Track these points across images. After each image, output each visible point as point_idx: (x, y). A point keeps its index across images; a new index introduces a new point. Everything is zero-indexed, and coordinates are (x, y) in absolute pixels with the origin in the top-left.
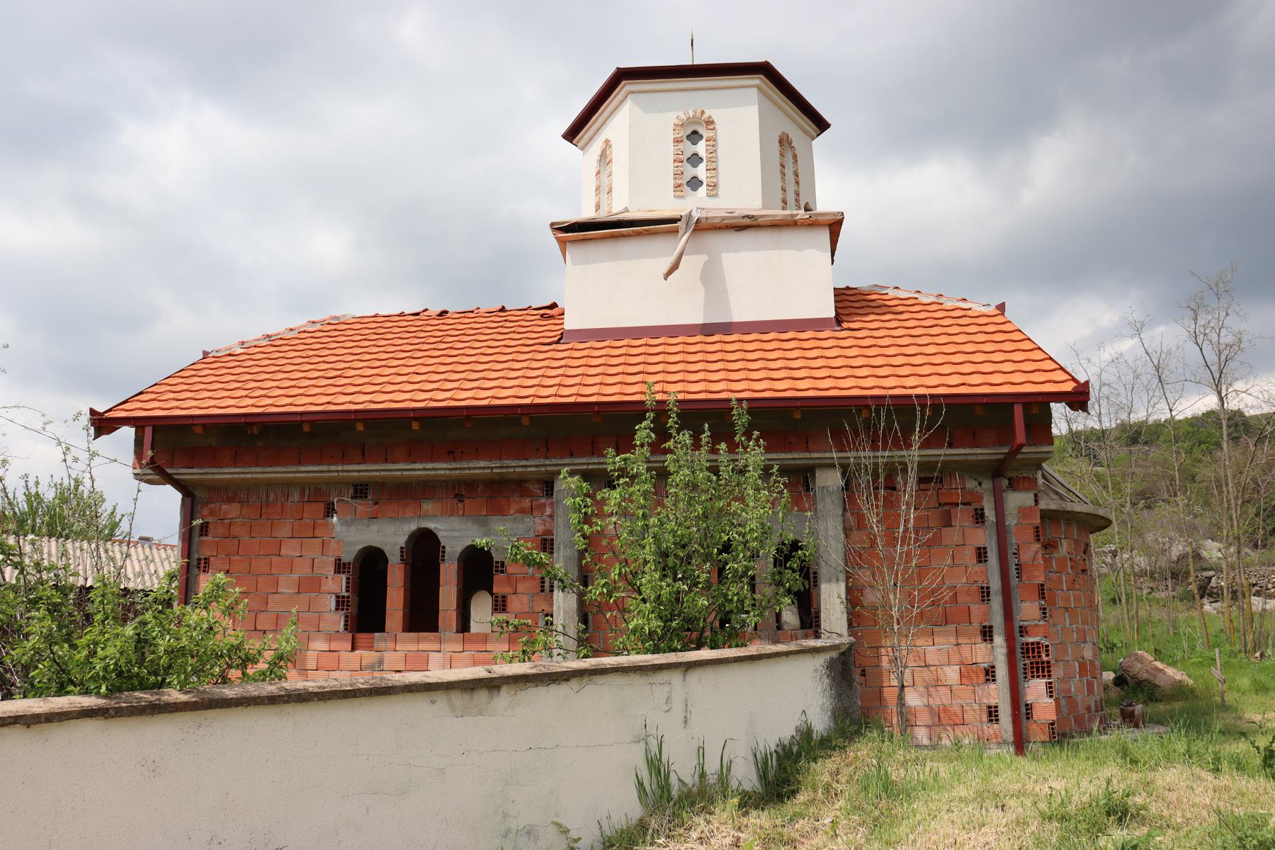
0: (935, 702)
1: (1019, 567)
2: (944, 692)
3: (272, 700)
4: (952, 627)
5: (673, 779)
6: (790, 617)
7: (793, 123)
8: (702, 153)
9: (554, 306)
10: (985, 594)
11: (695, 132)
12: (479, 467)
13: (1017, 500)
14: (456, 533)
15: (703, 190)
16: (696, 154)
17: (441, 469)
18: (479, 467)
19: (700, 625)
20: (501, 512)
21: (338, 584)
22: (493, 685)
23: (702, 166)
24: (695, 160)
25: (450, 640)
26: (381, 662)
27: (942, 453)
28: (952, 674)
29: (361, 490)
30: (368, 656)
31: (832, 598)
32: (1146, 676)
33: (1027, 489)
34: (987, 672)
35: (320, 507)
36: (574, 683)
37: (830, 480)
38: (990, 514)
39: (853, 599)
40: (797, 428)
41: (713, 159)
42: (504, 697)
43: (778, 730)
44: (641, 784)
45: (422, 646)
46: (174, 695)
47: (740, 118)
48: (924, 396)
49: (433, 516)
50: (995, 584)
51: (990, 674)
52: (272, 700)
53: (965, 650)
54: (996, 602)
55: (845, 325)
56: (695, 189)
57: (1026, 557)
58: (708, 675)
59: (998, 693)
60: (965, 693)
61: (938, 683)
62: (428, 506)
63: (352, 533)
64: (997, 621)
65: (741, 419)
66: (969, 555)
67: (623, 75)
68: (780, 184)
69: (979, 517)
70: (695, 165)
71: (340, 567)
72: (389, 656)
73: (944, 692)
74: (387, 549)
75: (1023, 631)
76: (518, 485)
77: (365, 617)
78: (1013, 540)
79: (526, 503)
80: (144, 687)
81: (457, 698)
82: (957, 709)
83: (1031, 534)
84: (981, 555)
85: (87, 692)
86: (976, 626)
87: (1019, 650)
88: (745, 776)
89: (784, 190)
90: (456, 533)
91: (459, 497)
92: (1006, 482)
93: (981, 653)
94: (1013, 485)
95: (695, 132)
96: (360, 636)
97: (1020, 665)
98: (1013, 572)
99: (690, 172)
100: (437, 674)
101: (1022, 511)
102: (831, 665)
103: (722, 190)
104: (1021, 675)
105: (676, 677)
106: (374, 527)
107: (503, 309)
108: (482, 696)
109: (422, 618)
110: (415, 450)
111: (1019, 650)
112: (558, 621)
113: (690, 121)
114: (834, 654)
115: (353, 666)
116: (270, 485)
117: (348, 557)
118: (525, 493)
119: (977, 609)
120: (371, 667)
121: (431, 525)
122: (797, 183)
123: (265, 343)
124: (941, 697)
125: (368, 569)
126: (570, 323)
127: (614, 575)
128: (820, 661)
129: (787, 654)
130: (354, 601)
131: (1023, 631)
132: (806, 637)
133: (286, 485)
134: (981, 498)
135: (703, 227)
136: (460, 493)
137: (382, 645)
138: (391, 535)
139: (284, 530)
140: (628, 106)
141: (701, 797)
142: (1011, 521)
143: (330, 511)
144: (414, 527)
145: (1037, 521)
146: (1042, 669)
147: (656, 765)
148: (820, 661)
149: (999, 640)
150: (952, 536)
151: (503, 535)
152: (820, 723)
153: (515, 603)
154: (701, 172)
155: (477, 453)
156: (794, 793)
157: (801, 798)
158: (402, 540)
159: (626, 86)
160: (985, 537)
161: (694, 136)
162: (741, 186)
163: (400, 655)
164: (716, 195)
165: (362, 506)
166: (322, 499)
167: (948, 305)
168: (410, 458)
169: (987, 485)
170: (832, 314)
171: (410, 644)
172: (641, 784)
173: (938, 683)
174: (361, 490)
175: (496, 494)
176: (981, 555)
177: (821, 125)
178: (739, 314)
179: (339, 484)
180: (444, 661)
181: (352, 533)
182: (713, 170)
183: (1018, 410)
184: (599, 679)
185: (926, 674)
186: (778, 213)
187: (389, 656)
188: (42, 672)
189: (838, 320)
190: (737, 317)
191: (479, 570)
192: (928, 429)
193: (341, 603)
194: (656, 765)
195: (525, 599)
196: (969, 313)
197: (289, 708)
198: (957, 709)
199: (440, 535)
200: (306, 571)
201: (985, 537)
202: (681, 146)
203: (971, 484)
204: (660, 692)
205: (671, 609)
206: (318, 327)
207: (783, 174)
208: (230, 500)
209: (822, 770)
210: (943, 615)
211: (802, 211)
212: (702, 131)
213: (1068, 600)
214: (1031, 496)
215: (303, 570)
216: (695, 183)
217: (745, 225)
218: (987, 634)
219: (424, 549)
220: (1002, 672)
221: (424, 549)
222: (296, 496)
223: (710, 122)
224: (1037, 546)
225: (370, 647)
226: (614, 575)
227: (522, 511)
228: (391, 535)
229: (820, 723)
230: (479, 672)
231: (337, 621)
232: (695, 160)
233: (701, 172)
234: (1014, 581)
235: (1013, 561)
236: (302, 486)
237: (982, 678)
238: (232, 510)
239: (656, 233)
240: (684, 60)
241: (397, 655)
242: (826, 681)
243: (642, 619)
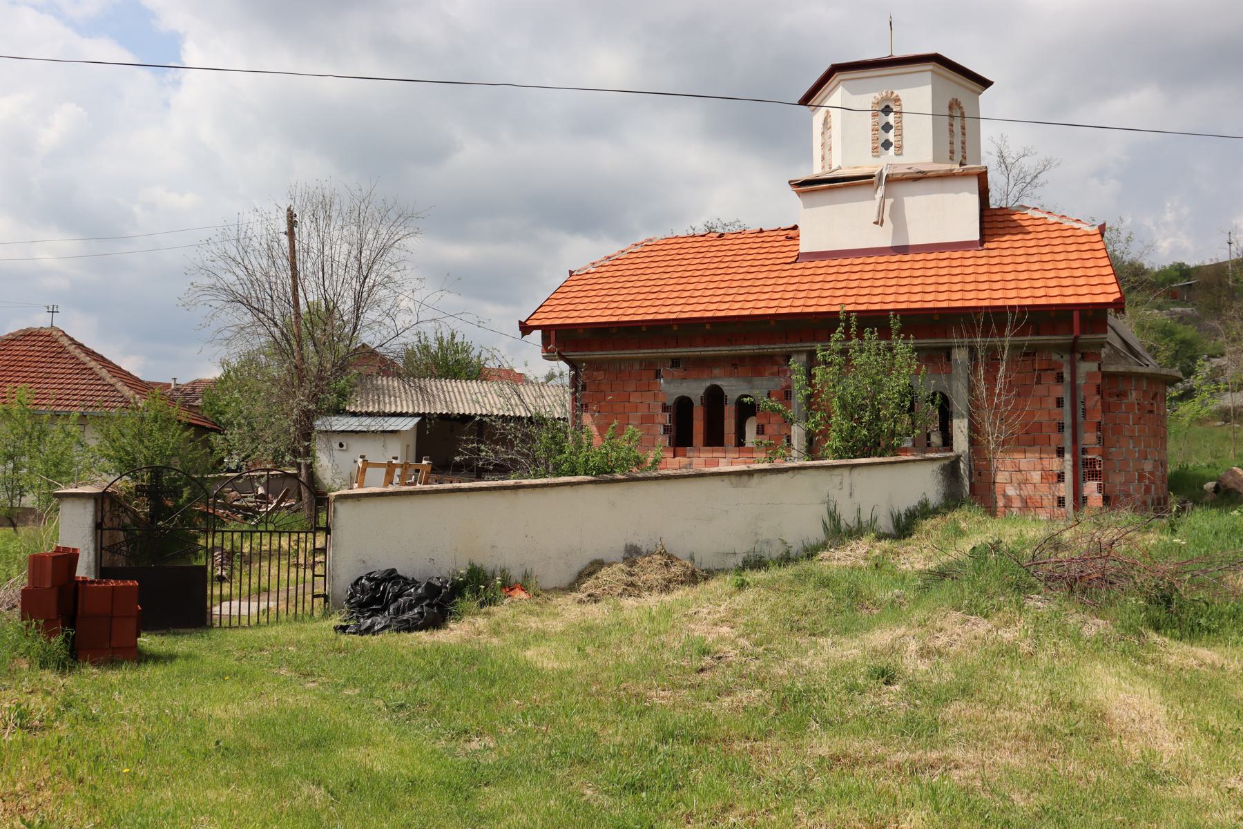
0: (1024, 493)
1: (1084, 411)
2: (1030, 487)
3: (656, 478)
4: (1037, 448)
5: (843, 523)
6: (936, 439)
7: (958, 88)
8: (892, 123)
9: (795, 228)
10: (1061, 427)
11: (887, 107)
12: (747, 349)
13: (1086, 368)
14: (733, 388)
15: (892, 149)
16: (888, 123)
17: (724, 350)
18: (747, 349)
19: (870, 443)
20: (760, 375)
21: (664, 419)
22: (750, 473)
23: (892, 132)
24: (887, 127)
25: (731, 451)
26: (691, 464)
27: (1028, 339)
28: (1036, 476)
29: (676, 362)
30: (683, 460)
31: (960, 427)
32: (1232, 485)
33: (1094, 360)
34: (1059, 476)
35: (652, 373)
36: (790, 473)
37: (960, 356)
38: (1067, 376)
39: (974, 429)
40: (932, 328)
41: (900, 128)
42: (756, 479)
43: (907, 501)
44: (825, 524)
45: (715, 455)
46: (618, 476)
47: (918, 95)
48: (1014, 307)
49: (720, 378)
50: (1068, 421)
51: (1061, 477)
52: (656, 478)
53: (1046, 462)
54: (1068, 433)
55: (986, 245)
56: (887, 149)
57: (1089, 404)
58: (865, 471)
59: (1066, 489)
60: (1044, 489)
61: (1026, 482)
62: (716, 371)
63: (672, 388)
64: (1068, 444)
65: (895, 324)
66: (1051, 403)
67: (836, 69)
68: (948, 140)
69: (1060, 378)
70: (887, 131)
71: (665, 408)
72: (695, 460)
73: (1030, 487)
74: (692, 398)
75: (1085, 451)
76: (771, 359)
77: (681, 439)
78: (1081, 394)
79: (775, 369)
80: (606, 473)
81: (733, 478)
82: (1038, 498)
83: (1094, 390)
84: (1060, 402)
85: (586, 474)
86: (1054, 447)
87: (1080, 463)
88: (885, 524)
89: (952, 143)
90: (733, 388)
91: (735, 366)
92: (1078, 356)
93: (1055, 464)
94: (1084, 358)
95: (887, 107)
96: (678, 449)
97: (1081, 472)
98: (1080, 413)
99: (883, 136)
100: (723, 467)
101: (1090, 375)
102: (944, 468)
103: (905, 150)
104: (1081, 478)
105: (846, 472)
106: (685, 385)
107: (761, 231)
108: (745, 478)
109: (714, 439)
110: (707, 340)
111: (1080, 463)
112: (794, 441)
113: (883, 100)
114: (947, 462)
115: (673, 464)
116: (621, 360)
117: (670, 402)
118: (775, 363)
119: (1055, 437)
120: (685, 467)
121: (719, 383)
122: (964, 134)
123: (607, 263)
124: (1028, 491)
125: (682, 408)
126: (805, 246)
127: (818, 417)
128: (936, 466)
129: (914, 461)
130: (674, 428)
131: (1085, 451)
132: (945, 451)
133: (631, 361)
134: (1062, 366)
135: (892, 180)
136: (735, 363)
137: (691, 454)
138: (695, 390)
139: (631, 386)
140: (840, 90)
141: (856, 533)
142: (1081, 381)
143: (658, 375)
144: (708, 384)
145: (1099, 381)
146: (1094, 475)
147: (833, 515)
148: (936, 466)
149: (1068, 456)
150: (1040, 390)
151: (758, 390)
152: (934, 498)
153: (770, 429)
154: (891, 136)
155: (745, 342)
156: (911, 535)
157: (914, 537)
158: (701, 392)
159: (839, 77)
160: (1063, 391)
161: (887, 110)
162: (919, 145)
163: (702, 460)
164: (901, 154)
165: (677, 372)
166: (653, 369)
167: (1067, 224)
168: (705, 344)
169: (1067, 357)
170: (977, 237)
171: (707, 454)
172: (825, 524)
173: (1026, 482)
174: (676, 362)
175: (756, 365)
176: (1060, 402)
177: (986, 83)
178: (913, 241)
179: (663, 359)
180: (727, 462)
181: (672, 388)
182: (899, 135)
183: (1076, 314)
184: (803, 472)
185: (1019, 476)
186: (944, 167)
187: (695, 460)
188: (565, 467)
189: (983, 241)
190: (912, 243)
191: (746, 410)
192: (1016, 326)
193: (666, 429)
194: (833, 515)
195: (775, 427)
196: (1078, 233)
197: (662, 482)
198: (1038, 498)
199: (724, 389)
200: (645, 412)
201: (1063, 391)
202: (877, 119)
203: (1055, 357)
204: (837, 479)
205: (848, 437)
206: (639, 249)
207: (951, 131)
208: (598, 369)
209: (928, 524)
210: (1029, 439)
211: (957, 166)
212: (892, 106)
213: (1133, 431)
214: (1096, 365)
215: (643, 410)
216: (887, 145)
217: (920, 177)
218: (1060, 452)
219: (715, 397)
220: (1069, 476)
221: (715, 397)
222: (637, 367)
223: (897, 100)
224: (1098, 397)
225: (685, 456)
226: (818, 417)
227: (773, 374)
228: (695, 390)
229: (934, 498)
230: (744, 467)
231: (663, 440)
232: (887, 127)
233: (891, 136)
234: (1080, 419)
235: (1080, 407)
236: (641, 360)
237: (1055, 479)
238: (600, 375)
239: (859, 185)
240: (882, 54)
241: (700, 459)
242: (940, 477)
243: (834, 441)
